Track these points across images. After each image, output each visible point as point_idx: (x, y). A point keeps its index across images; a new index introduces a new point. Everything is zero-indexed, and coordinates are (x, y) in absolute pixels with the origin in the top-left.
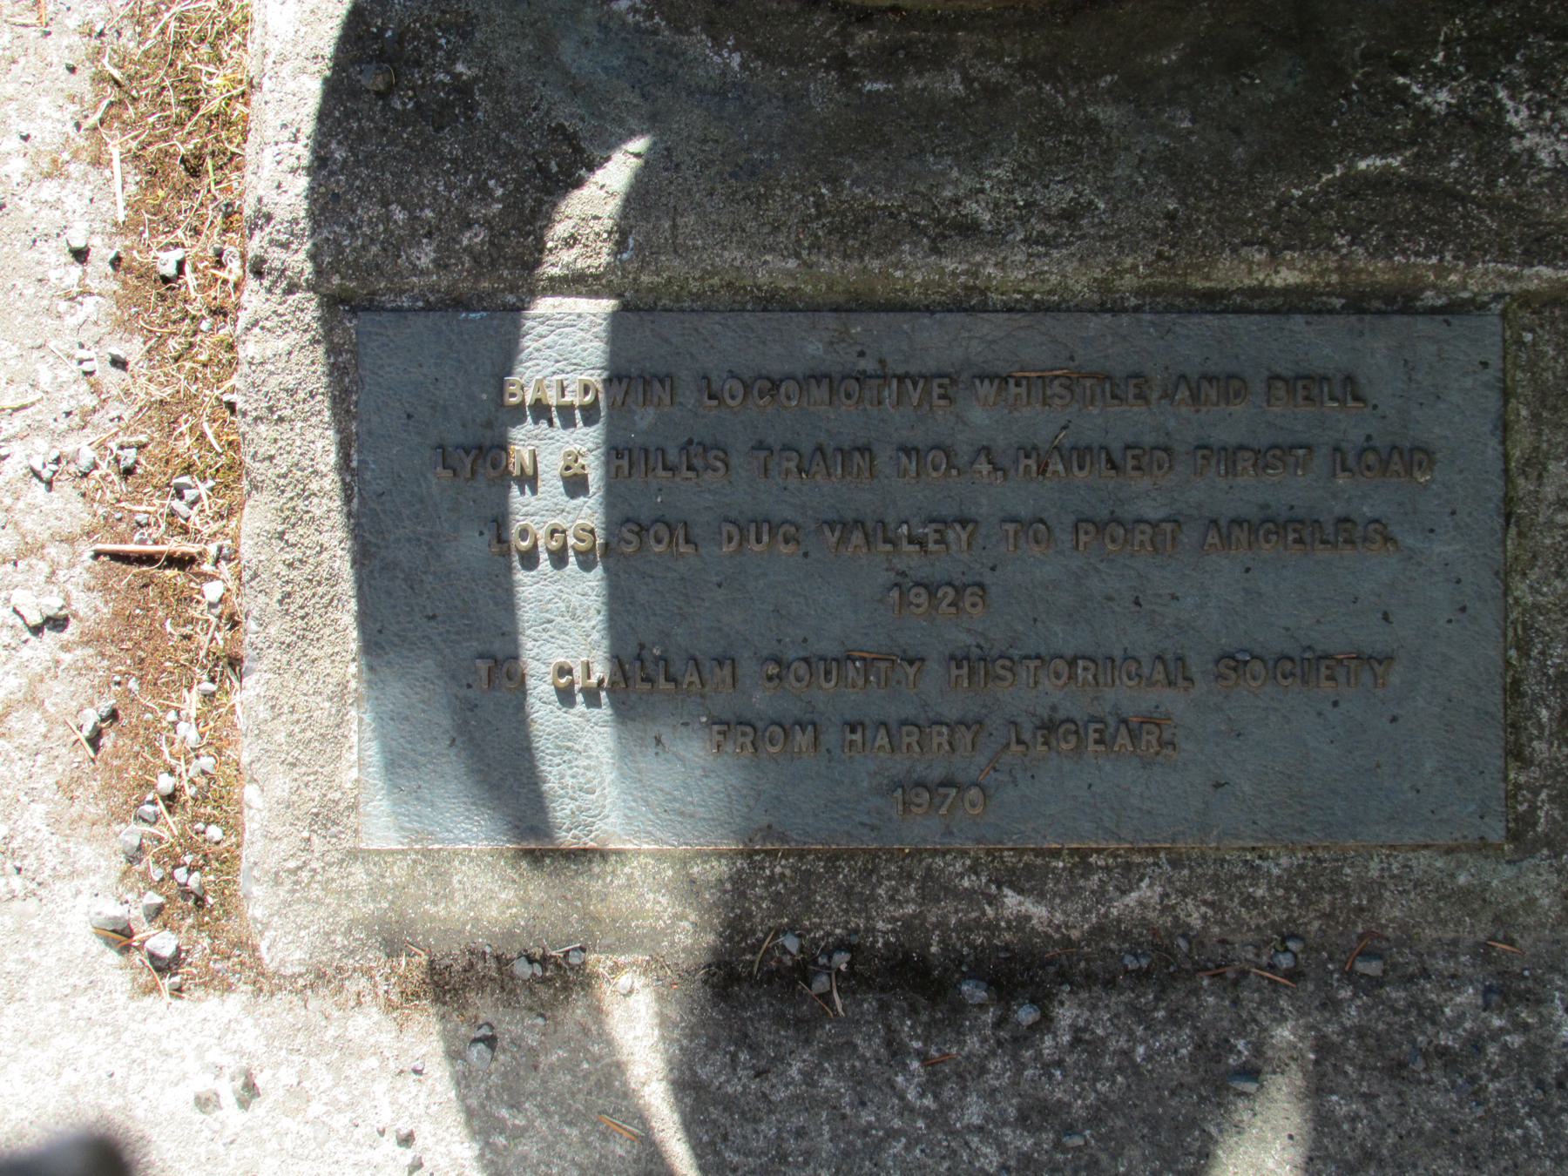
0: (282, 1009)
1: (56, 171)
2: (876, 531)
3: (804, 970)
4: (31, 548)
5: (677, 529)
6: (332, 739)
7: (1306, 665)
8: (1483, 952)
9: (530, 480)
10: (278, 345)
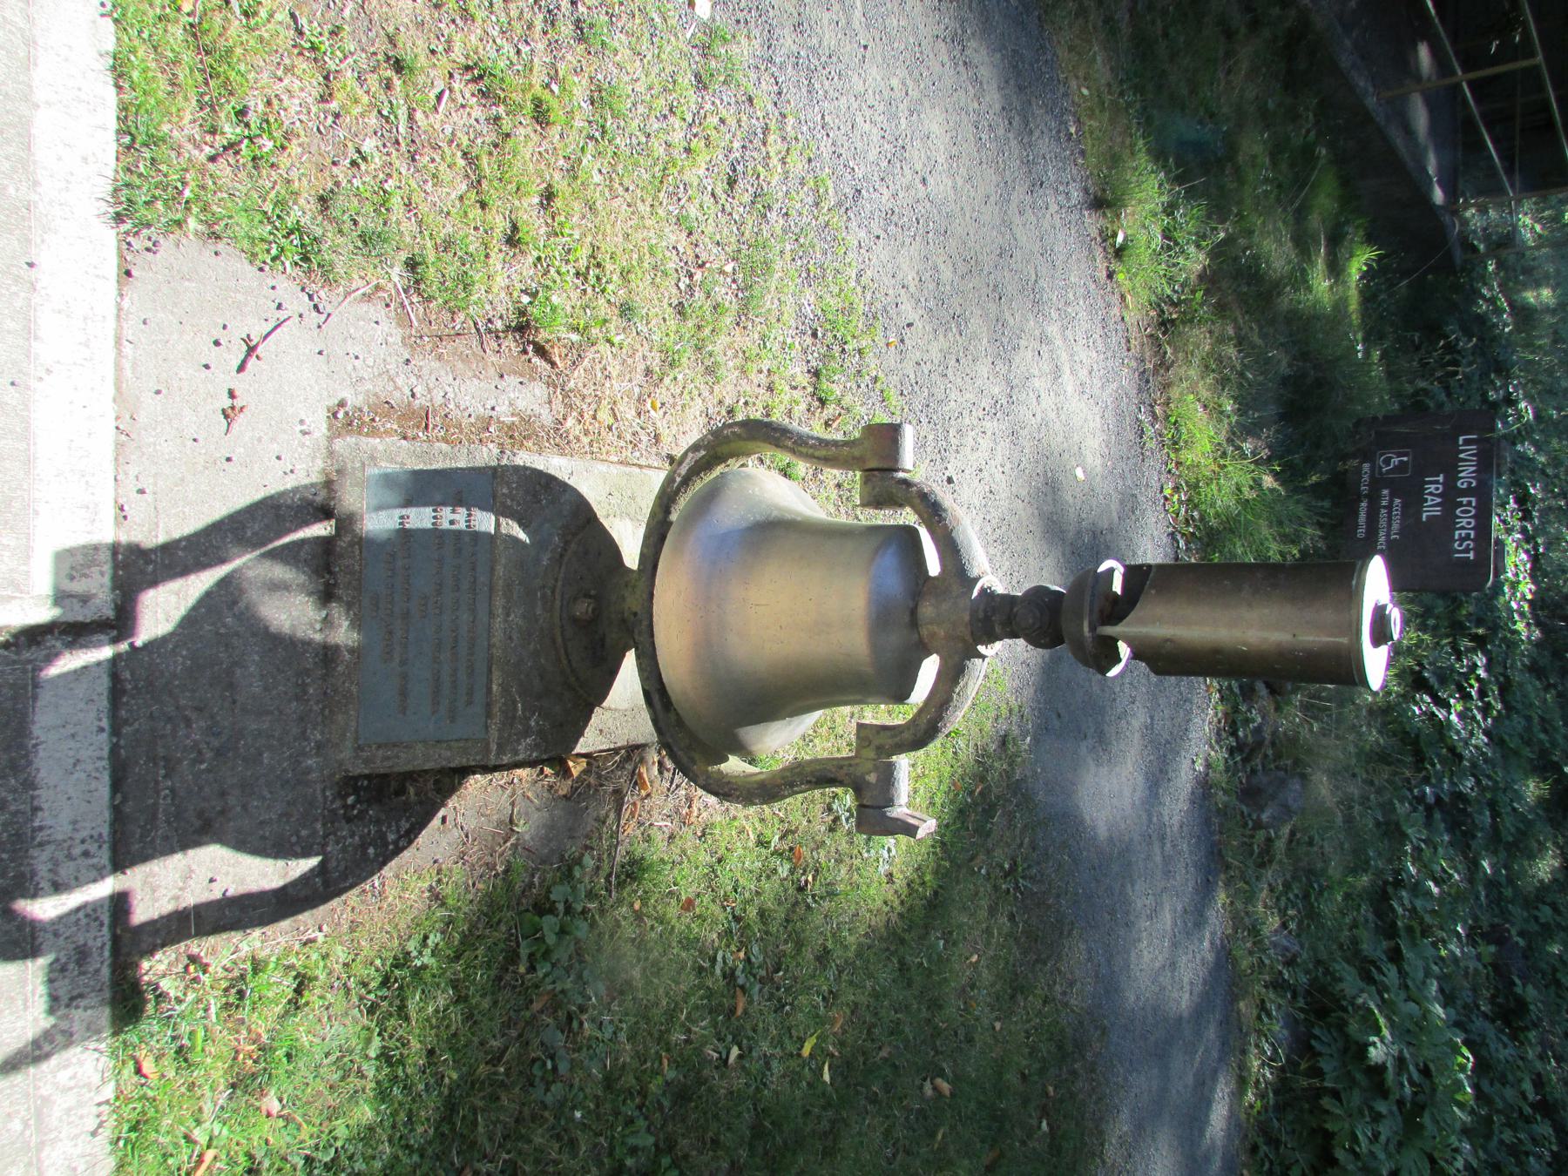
0: (323, 443)
1: (511, 404)
2: (439, 593)
3: (330, 573)
4: (429, 391)
5: (441, 546)
6: (392, 461)
7: (404, 693)
8: (329, 741)
9: (453, 512)
10: (486, 455)
